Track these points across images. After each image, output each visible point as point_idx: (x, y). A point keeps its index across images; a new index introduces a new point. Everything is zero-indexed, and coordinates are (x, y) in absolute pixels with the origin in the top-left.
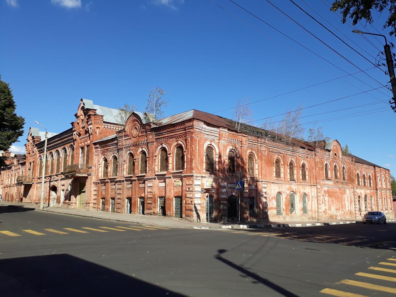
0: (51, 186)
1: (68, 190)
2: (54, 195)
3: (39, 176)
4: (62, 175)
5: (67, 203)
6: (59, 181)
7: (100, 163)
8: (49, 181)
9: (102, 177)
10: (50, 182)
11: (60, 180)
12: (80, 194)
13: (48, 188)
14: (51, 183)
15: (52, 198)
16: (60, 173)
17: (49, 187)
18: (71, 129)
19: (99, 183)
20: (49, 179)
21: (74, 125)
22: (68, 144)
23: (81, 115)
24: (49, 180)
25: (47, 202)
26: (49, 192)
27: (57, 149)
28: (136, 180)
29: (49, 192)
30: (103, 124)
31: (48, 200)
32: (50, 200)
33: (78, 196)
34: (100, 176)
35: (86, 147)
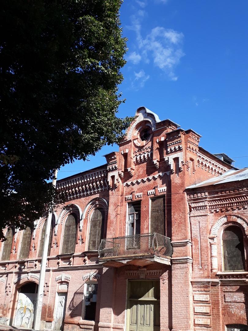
0: (22, 282)
1: (82, 293)
2: (24, 302)
3: (66, 253)
4: (60, 260)
5: (79, 325)
6: (14, 274)
7: (211, 236)
8: (16, 273)
9: (223, 269)
10: (19, 274)
11: (54, 271)
12: (130, 307)
13: (13, 287)
14: (23, 276)
15: (18, 308)
16: (54, 256)
17: (17, 283)
18: (105, 166)
19: (214, 284)
20: (16, 267)
21: (180, 137)
22: (80, 197)
23: (135, 140)
24: (17, 270)
25: (9, 315)
26: (15, 295)
27: (76, 203)
28: (218, 283)
29: (15, 295)
30: (198, 155)
31: (11, 310)
32: (15, 312)
33: (126, 310)
34: (215, 265)
35: (150, 201)
